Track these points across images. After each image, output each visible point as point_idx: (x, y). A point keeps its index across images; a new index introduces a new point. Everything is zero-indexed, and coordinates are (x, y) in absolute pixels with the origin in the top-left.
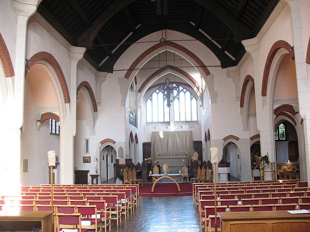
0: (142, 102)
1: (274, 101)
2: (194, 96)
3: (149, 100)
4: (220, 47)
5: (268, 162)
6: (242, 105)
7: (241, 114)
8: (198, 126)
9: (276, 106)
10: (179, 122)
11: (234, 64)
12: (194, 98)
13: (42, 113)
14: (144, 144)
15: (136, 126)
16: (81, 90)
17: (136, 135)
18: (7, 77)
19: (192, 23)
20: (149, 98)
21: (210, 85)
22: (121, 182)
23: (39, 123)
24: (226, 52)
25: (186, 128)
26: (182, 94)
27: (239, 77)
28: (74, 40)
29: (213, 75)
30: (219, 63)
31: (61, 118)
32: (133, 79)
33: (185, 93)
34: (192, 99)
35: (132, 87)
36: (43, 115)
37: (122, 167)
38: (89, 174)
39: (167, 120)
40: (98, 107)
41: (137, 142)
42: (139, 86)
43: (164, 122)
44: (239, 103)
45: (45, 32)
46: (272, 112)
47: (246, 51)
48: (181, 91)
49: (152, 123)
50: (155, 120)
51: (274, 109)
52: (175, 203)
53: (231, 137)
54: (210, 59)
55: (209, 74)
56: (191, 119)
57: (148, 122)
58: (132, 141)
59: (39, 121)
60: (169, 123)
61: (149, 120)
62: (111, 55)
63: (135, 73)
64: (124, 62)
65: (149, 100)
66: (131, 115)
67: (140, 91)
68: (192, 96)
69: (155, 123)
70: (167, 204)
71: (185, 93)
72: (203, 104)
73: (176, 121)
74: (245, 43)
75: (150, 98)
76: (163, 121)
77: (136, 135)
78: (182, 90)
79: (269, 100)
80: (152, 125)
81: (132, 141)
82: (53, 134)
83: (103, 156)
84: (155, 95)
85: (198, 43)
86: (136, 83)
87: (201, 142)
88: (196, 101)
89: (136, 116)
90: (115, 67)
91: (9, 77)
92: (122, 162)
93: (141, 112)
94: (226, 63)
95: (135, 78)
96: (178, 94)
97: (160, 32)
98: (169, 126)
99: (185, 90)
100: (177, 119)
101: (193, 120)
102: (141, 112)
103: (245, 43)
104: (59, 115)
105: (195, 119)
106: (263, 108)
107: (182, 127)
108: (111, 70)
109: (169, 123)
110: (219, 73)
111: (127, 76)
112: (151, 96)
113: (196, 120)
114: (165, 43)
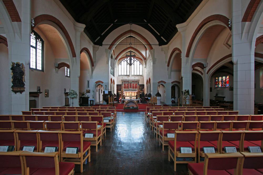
1: (193, 60)
3: (120, 64)
4: (159, 34)
5: (189, 94)
6: (168, 66)
9: (193, 63)
11: (166, 44)
12: (141, 64)
13: (59, 63)
14: (117, 85)
15: (114, 76)
16: (82, 53)
17: (114, 80)
18: (13, 21)
19: (145, 20)
20: (120, 64)
21: (153, 54)
23: (57, 69)
24: (162, 37)
25: (137, 78)
26: (135, 62)
28: (78, 19)
29: (154, 49)
30: (157, 43)
32: (113, 51)
34: (140, 64)
35: (112, 57)
36: (59, 64)
37: (107, 95)
38: (89, 99)
42: (115, 56)
43: (127, 75)
47: (178, 31)
49: (121, 75)
50: (123, 74)
52: (134, 116)
54: (153, 40)
55: (152, 49)
56: (140, 74)
58: (112, 83)
59: (57, 67)
61: (120, 74)
62: (101, 36)
63: (114, 48)
64: (108, 41)
65: (120, 64)
67: (116, 59)
72: (146, 66)
73: (132, 74)
74: (178, 26)
76: (126, 75)
77: (114, 80)
78: (136, 60)
80: (121, 77)
81: (112, 83)
83: (97, 90)
84: (123, 62)
88: (142, 66)
89: (114, 71)
90: (103, 43)
91: (15, 21)
92: (107, 92)
93: (116, 69)
94: (161, 43)
95: (114, 50)
96: (134, 62)
97: (128, 25)
98: (129, 77)
99: (137, 60)
100: (133, 74)
101: (140, 75)
102: (116, 69)
103: (178, 26)
104: (69, 64)
105: (141, 74)
108: (101, 45)
109: (129, 76)
110: (157, 48)
111: (110, 48)
112: (121, 62)
113: (142, 75)
114: (131, 31)
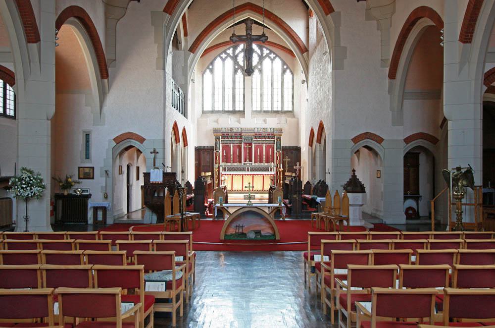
0: (195, 73)
2: (288, 68)
3: (208, 71)
5: (471, 183)
6: (392, 75)
7: (390, 91)
8: (294, 119)
10: (260, 112)
12: (288, 71)
14: (198, 150)
15: (185, 114)
16: (64, 27)
17: (184, 130)
20: (208, 68)
22: (155, 218)
27: (391, 18)
29: (339, 13)
31: (19, 77)
32: (180, 20)
33: (272, 60)
34: (284, 72)
35: (176, 43)
39: (239, 107)
40: (110, 70)
41: (185, 144)
42: (191, 40)
43: (234, 112)
44: (387, 70)
45: (83, 35)
46: (481, 78)
48: (266, 56)
49: (213, 112)
50: (219, 107)
51: (486, 70)
53: (367, 135)
57: (205, 109)
60: (242, 113)
61: (208, 108)
65: (208, 71)
66: (176, 92)
67: (193, 49)
68: (285, 67)
69: (218, 112)
70: (243, 258)
71: (272, 60)
72: (307, 78)
75: (211, 67)
77: (184, 130)
78: (268, 55)
79: (478, 50)
80: (214, 117)
81: (177, 141)
82: (10, 117)
83: (120, 167)
85: (272, 24)
86: (186, 34)
87: (298, 150)
88: (291, 76)
95: (184, 18)
98: (242, 120)
99: (272, 56)
100: (257, 106)
102: (193, 89)
104: (13, 71)
105: (288, 107)
106: (461, 69)
107: (265, 121)
109: (242, 113)
112: (212, 63)
113: (290, 109)
